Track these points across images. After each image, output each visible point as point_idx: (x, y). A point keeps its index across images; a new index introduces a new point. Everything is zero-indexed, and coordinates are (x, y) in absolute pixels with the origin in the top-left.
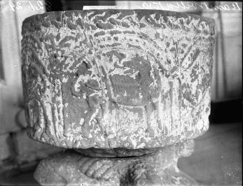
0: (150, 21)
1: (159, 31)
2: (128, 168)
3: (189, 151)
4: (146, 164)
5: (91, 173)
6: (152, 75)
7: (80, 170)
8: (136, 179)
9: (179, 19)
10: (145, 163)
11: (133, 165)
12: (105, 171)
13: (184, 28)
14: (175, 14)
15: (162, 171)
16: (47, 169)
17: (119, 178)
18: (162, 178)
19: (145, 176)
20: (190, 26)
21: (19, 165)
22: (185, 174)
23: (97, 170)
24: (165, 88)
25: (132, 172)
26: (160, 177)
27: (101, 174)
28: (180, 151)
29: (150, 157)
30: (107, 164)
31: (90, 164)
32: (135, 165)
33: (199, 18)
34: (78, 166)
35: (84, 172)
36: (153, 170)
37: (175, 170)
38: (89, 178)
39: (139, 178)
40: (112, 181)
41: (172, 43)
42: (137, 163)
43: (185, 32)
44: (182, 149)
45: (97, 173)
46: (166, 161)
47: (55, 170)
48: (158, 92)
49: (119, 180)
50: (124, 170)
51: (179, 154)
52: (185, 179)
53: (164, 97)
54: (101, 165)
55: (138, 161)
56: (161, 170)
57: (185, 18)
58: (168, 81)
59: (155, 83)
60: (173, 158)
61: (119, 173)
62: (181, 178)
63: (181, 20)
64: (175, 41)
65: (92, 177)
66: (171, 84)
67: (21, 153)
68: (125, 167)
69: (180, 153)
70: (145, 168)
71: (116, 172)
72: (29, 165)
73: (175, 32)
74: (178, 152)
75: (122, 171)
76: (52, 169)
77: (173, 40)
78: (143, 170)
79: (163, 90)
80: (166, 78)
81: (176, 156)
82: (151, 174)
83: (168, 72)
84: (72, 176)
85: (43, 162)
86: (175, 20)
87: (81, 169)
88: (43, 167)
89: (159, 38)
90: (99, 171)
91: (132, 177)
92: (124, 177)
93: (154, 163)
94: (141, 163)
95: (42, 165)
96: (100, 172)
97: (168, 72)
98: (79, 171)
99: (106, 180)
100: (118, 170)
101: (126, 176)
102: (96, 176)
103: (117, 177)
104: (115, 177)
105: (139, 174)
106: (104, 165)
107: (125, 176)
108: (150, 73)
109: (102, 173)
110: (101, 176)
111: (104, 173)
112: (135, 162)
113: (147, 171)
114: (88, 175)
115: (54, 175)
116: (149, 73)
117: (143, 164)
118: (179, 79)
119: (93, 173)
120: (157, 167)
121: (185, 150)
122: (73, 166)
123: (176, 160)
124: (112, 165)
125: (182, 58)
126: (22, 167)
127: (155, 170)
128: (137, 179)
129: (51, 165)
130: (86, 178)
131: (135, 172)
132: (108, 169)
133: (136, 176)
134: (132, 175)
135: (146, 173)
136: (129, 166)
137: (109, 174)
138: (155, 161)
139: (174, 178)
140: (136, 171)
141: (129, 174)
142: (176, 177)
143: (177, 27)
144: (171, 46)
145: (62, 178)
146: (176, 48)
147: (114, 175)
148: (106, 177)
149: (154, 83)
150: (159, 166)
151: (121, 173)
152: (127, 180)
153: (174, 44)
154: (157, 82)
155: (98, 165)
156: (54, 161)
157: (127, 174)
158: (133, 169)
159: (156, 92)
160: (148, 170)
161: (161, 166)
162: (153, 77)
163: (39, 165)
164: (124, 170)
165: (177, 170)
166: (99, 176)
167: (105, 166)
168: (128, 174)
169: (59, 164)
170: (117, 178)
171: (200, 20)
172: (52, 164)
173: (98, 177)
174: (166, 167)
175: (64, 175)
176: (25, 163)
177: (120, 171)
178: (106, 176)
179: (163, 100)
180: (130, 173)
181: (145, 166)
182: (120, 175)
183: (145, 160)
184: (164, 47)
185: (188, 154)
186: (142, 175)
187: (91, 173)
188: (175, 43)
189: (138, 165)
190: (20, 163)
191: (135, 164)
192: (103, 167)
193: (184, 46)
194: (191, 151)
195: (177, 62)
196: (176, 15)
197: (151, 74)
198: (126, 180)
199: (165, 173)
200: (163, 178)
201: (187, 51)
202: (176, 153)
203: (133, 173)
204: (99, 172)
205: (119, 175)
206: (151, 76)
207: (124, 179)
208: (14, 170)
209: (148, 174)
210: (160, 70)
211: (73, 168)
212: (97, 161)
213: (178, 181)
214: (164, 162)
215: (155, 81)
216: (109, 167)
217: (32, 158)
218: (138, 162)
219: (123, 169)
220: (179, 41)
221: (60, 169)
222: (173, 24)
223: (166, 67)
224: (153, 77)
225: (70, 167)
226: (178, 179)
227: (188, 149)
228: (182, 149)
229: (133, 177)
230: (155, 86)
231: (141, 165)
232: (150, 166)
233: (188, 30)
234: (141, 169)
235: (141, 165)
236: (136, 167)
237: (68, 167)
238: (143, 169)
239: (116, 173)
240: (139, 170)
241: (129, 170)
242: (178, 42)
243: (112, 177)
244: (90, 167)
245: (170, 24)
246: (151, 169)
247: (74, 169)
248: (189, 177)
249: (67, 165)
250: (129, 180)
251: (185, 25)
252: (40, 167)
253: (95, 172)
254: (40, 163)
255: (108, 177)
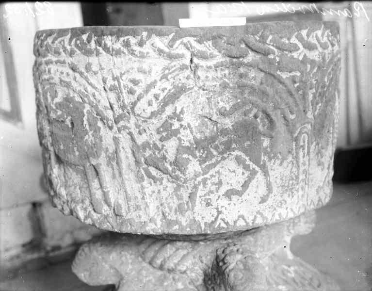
0: (80, 45)
1: (93, 60)
2: (215, 254)
3: (307, 225)
4: (243, 246)
5: (159, 262)
6: (86, 125)
7: (142, 257)
8: (227, 270)
9: (122, 39)
10: (241, 246)
11: (222, 249)
12: (180, 259)
13: (132, 53)
14: (116, 32)
15: (267, 258)
16: (92, 257)
17: (201, 270)
18: (267, 269)
19: (241, 266)
20: (147, 48)
21: (47, 252)
22: (304, 263)
23: (168, 258)
24: (109, 145)
25: (221, 258)
26: (264, 267)
27: (174, 263)
28: (294, 226)
29: (248, 236)
30: (183, 248)
31: (157, 249)
32: (227, 248)
33: (173, 32)
34: (138, 252)
35: (148, 261)
36: (255, 256)
37: (286, 255)
38: (155, 270)
39: (233, 269)
40: (191, 273)
41: (110, 78)
42: (228, 245)
43: (136, 59)
44: (297, 223)
45: (168, 262)
46: (274, 242)
47: (103, 258)
48: (95, 150)
49: (201, 272)
50: (209, 257)
51: (292, 231)
52: (302, 269)
53: (110, 160)
54: (174, 249)
55: (231, 243)
56: (266, 255)
57: (134, 37)
58: (112, 136)
59: (91, 136)
60: (283, 237)
61: (202, 262)
62: (296, 268)
63: (126, 40)
64: (115, 74)
65: (161, 267)
66: (116, 140)
67: (49, 233)
68: (211, 252)
69: (293, 229)
70: (242, 253)
71: (197, 260)
72: (62, 251)
73: (117, 60)
74: (291, 228)
75: (206, 258)
76: (100, 257)
77: (113, 74)
78: (239, 257)
79: (107, 148)
80: (110, 131)
81: (289, 234)
82: (250, 262)
83: (111, 122)
84: (130, 267)
85: (86, 247)
86: (116, 42)
87: (143, 256)
88: (86, 254)
89: (90, 70)
90: (170, 258)
91: (221, 267)
92: (209, 268)
93: (255, 246)
94: (235, 245)
95: (83, 250)
96: (173, 260)
97: (111, 122)
98: (140, 259)
99: (181, 273)
100: (200, 257)
101: (213, 266)
102: (166, 266)
103: (199, 267)
104: (196, 268)
105: (233, 263)
106: (177, 249)
107: (211, 266)
108: (83, 121)
109: (176, 261)
110: (174, 267)
111: (179, 261)
112: (226, 243)
113: (245, 258)
114: (155, 266)
115: (102, 266)
116: (83, 122)
117: (238, 247)
118: (130, 134)
119: (162, 262)
120: (261, 252)
121: (302, 224)
122: (130, 252)
123: (288, 239)
124: (190, 250)
125: (133, 101)
126: (51, 254)
127: (257, 255)
128: (230, 271)
129: (97, 251)
130: (151, 269)
131: (227, 260)
132: (184, 256)
133: (228, 266)
134: (221, 264)
135: (244, 260)
136: (217, 251)
137: (186, 264)
138: (256, 242)
139: (286, 268)
140: (228, 258)
141: (218, 263)
142: (289, 266)
143: (118, 53)
144: (110, 82)
145: (115, 270)
146: (118, 86)
147: (194, 264)
148: (183, 268)
149: (89, 136)
150: (262, 250)
151: (205, 262)
152: (214, 272)
153: (114, 79)
154: (93, 136)
155: (168, 250)
156: (101, 246)
157: (213, 262)
158: (223, 256)
159: (93, 150)
160: (247, 255)
161: (266, 249)
162: (87, 127)
163: (79, 252)
164: (209, 257)
165: (290, 256)
166: (172, 267)
167: (180, 251)
168: (215, 262)
169: (110, 248)
170: (199, 268)
171: (174, 36)
172: (100, 248)
173: (170, 268)
174: (273, 252)
175: (117, 266)
176: (57, 248)
177: (203, 258)
178: (182, 266)
179: (109, 164)
180: (218, 261)
181: (241, 250)
182: (204, 265)
183: (241, 241)
184: (100, 86)
185: (306, 231)
186: (237, 263)
187: (159, 262)
188: (116, 78)
189: (231, 248)
190: (49, 248)
191: (226, 247)
192: (177, 252)
193: (135, 82)
194: (311, 226)
195: (123, 107)
196: (117, 33)
197: (85, 122)
198: (212, 272)
199: (272, 259)
200: (269, 268)
201: (143, 91)
202: (289, 230)
203: (223, 260)
204: (171, 261)
205: (201, 264)
206: (84, 126)
207: (210, 270)
208: (40, 259)
209: (246, 262)
210: (99, 117)
211: (131, 254)
212: (167, 243)
213: (292, 272)
214: (269, 243)
215: (91, 133)
216: (185, 252)
217: (67, 241)
218: (230, 245)
219: (208, 255)
220: (122, 75)
221: (111, 257)
222: (111, 47)
223: (109, 114)
224: (87, 127)
225: (126, 253)
226: (292, 269)
227: (306, 223)
228: (297, 223)
229: (224, 268)
230: (91, 140)
231: (235, 249)
232: (248, 249)
233: (142, 56)
234: (235, 255)
235: (235, 249)
236: (228, 251)
237: (123, 253)
238: (238, 254)
239: (197, 261)
240: (232, 257)
241: (217, 257)
242: (121, 77)
243: (190, 267)
244: (157, 252)
245: (106, 49)
246: (250, 254)
247: (133, 256)
248: (309, 266)
249: (122, 251)
250: (217, 271)
251: (137, 49)
252: (80, 254)
253: (164, 261)
254: (81, 248)
255: (185, 268)
